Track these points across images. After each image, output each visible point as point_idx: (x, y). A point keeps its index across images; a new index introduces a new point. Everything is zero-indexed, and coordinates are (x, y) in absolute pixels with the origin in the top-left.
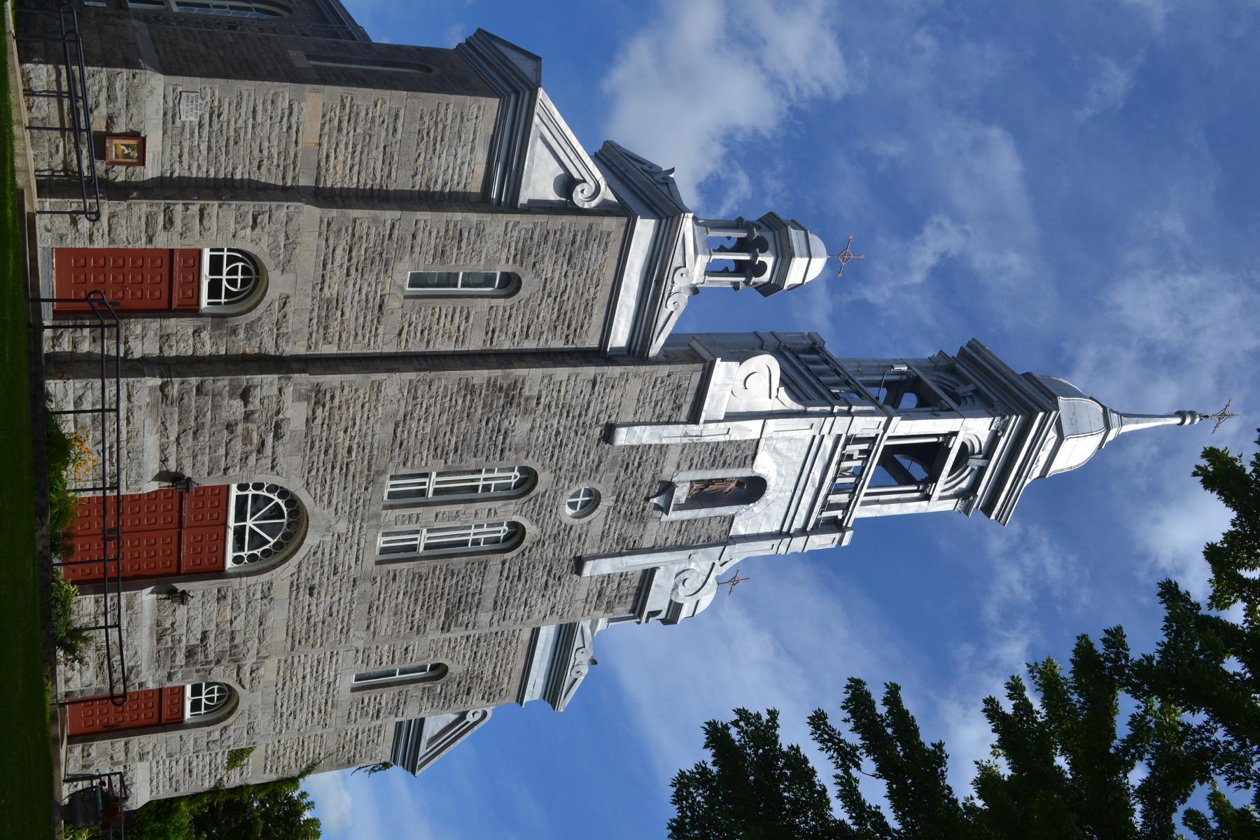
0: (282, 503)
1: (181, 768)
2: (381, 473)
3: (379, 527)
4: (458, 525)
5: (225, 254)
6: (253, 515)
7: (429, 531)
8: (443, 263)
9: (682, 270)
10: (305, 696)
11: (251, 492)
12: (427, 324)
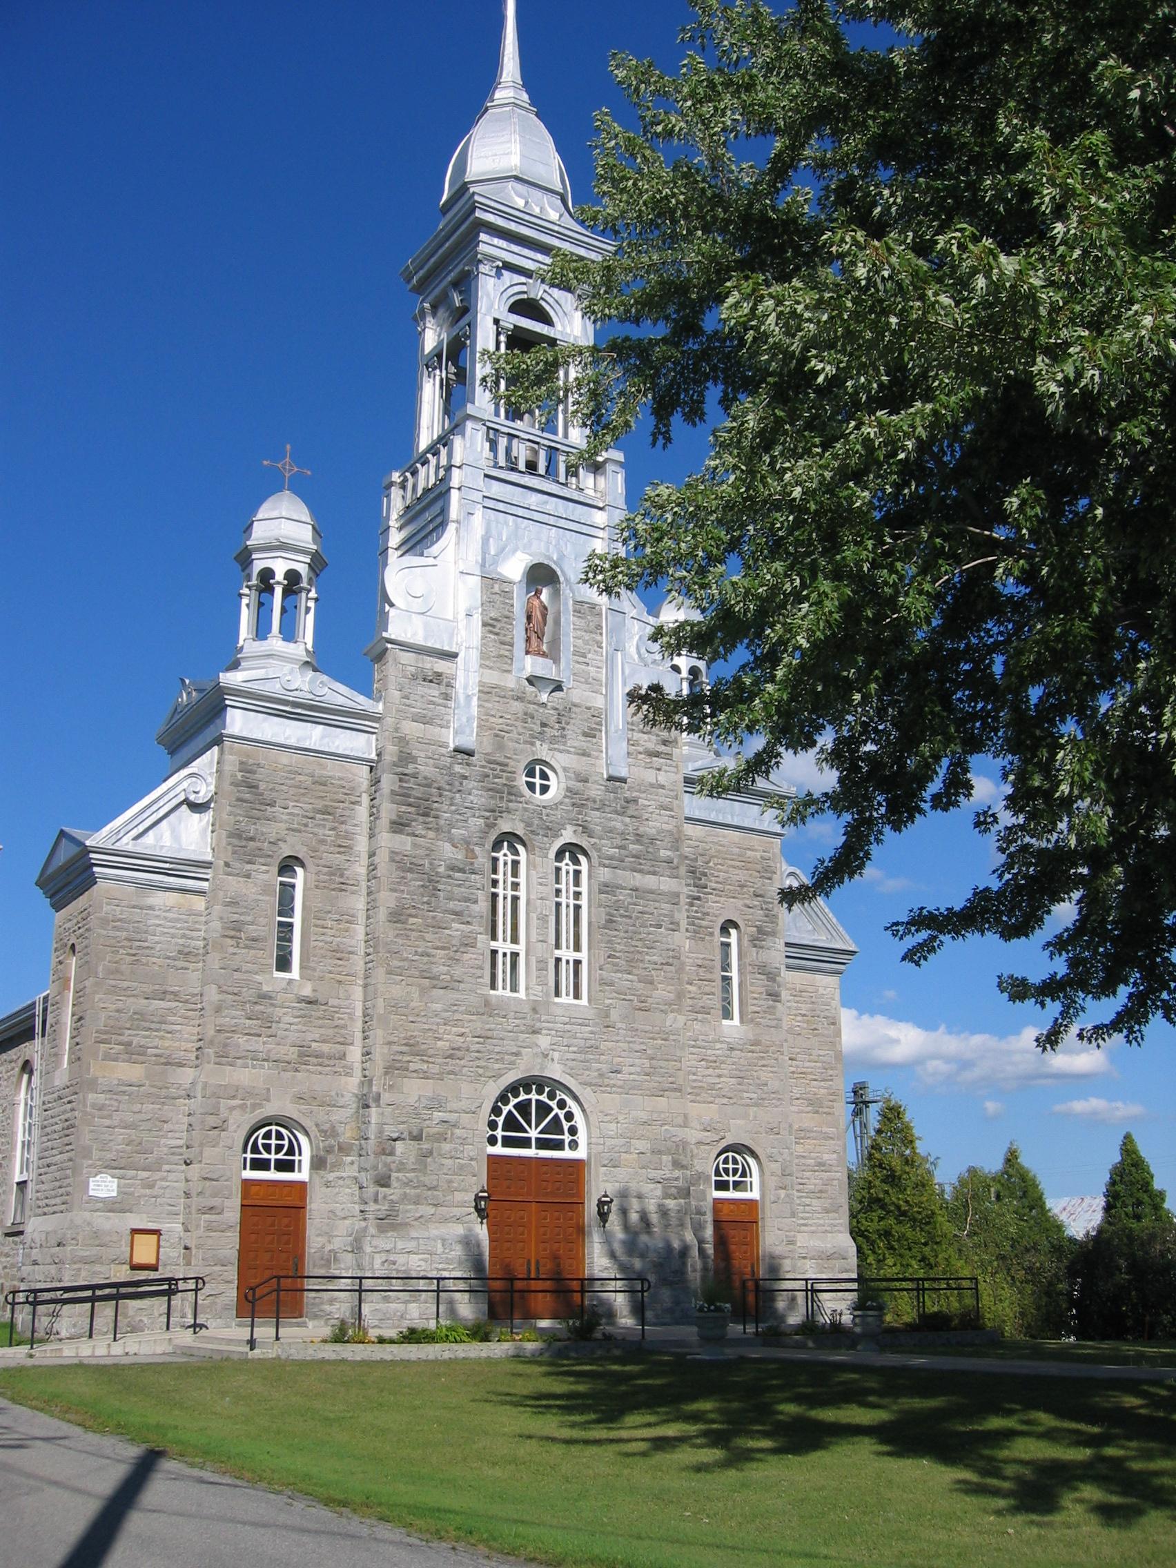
0: (514, 1101)
1: (814, 1202)
2: (487, 1003)
3: (548, 1003)
4: (553, 918)
5: (249, 1156)
6: (526, 1132)
7: (558, 946)
8: (264, 939)
9: (192, 797)
10: (742, 1074)
11: (499, 1133)
12: (329, 954)
